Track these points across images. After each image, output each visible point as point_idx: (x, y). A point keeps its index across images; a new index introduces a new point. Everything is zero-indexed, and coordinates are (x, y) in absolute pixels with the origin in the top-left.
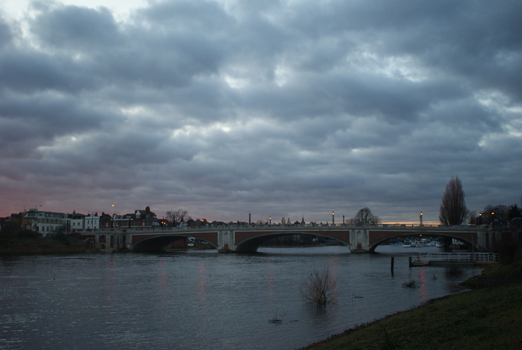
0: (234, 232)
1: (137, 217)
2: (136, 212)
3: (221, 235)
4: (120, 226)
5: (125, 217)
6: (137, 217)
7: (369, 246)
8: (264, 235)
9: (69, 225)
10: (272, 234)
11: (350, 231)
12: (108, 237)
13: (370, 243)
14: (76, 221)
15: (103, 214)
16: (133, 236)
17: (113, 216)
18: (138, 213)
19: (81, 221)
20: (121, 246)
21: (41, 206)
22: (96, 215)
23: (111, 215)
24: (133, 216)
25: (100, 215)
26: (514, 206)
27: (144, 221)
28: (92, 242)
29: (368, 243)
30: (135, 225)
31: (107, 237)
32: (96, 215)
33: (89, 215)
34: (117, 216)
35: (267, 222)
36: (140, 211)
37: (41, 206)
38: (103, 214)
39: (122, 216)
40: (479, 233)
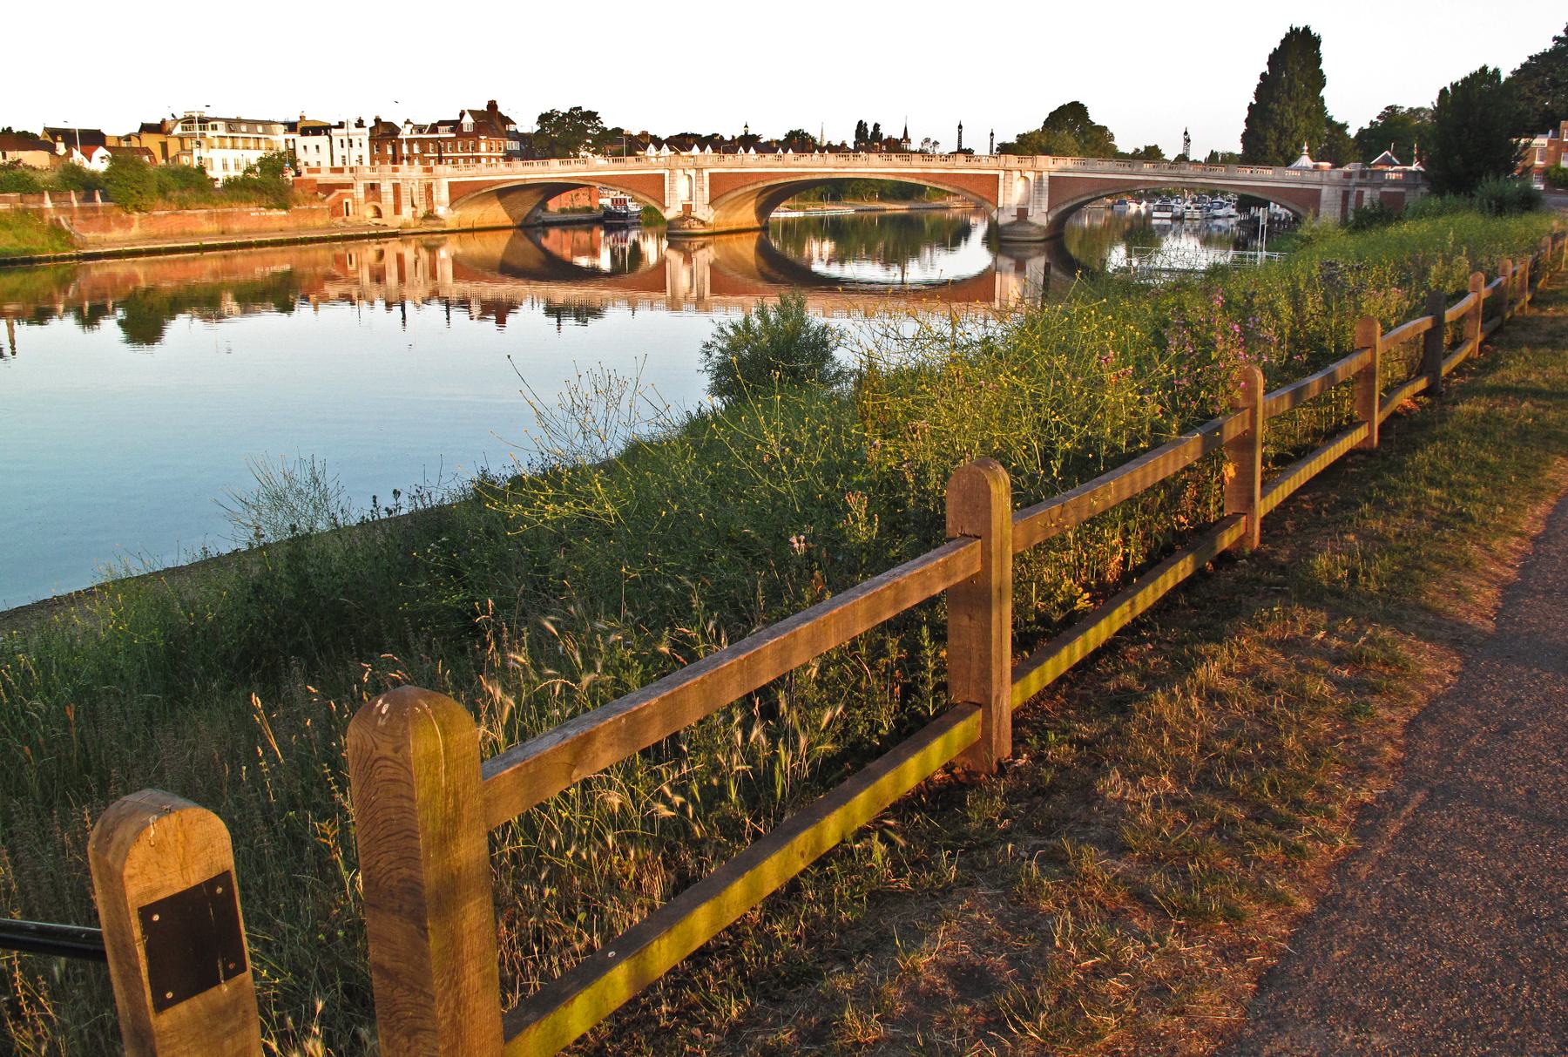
0: (706, 173)
2: (462, 115)
3: (672, 181)
5: (434, 128)
7: (1047, 213)
8: (782, 181)
9: (291, 157)
10: (802, 178)
11: (1002, 174)
12: (386, 188)
13: (1050, 208)
14: (311, 141)
15: (377, 120)
16: (450, 183)
19: (322, 140)
20: (422, 211)
21: (317, 147)
22: (360, 124)
23: (400, 124)
24: (455, 125)
25: (370, 123)
26: (1491, 69)
28: (346, 200)
29: (1045, 208)
31: (383, 189)
32: (360, 124)
33: (341, 125)
35: (978, 568)
36: (471, 112)
37: (317, 147)
38: (377, 120)
39: (426, 127)
40: (1325, 190)
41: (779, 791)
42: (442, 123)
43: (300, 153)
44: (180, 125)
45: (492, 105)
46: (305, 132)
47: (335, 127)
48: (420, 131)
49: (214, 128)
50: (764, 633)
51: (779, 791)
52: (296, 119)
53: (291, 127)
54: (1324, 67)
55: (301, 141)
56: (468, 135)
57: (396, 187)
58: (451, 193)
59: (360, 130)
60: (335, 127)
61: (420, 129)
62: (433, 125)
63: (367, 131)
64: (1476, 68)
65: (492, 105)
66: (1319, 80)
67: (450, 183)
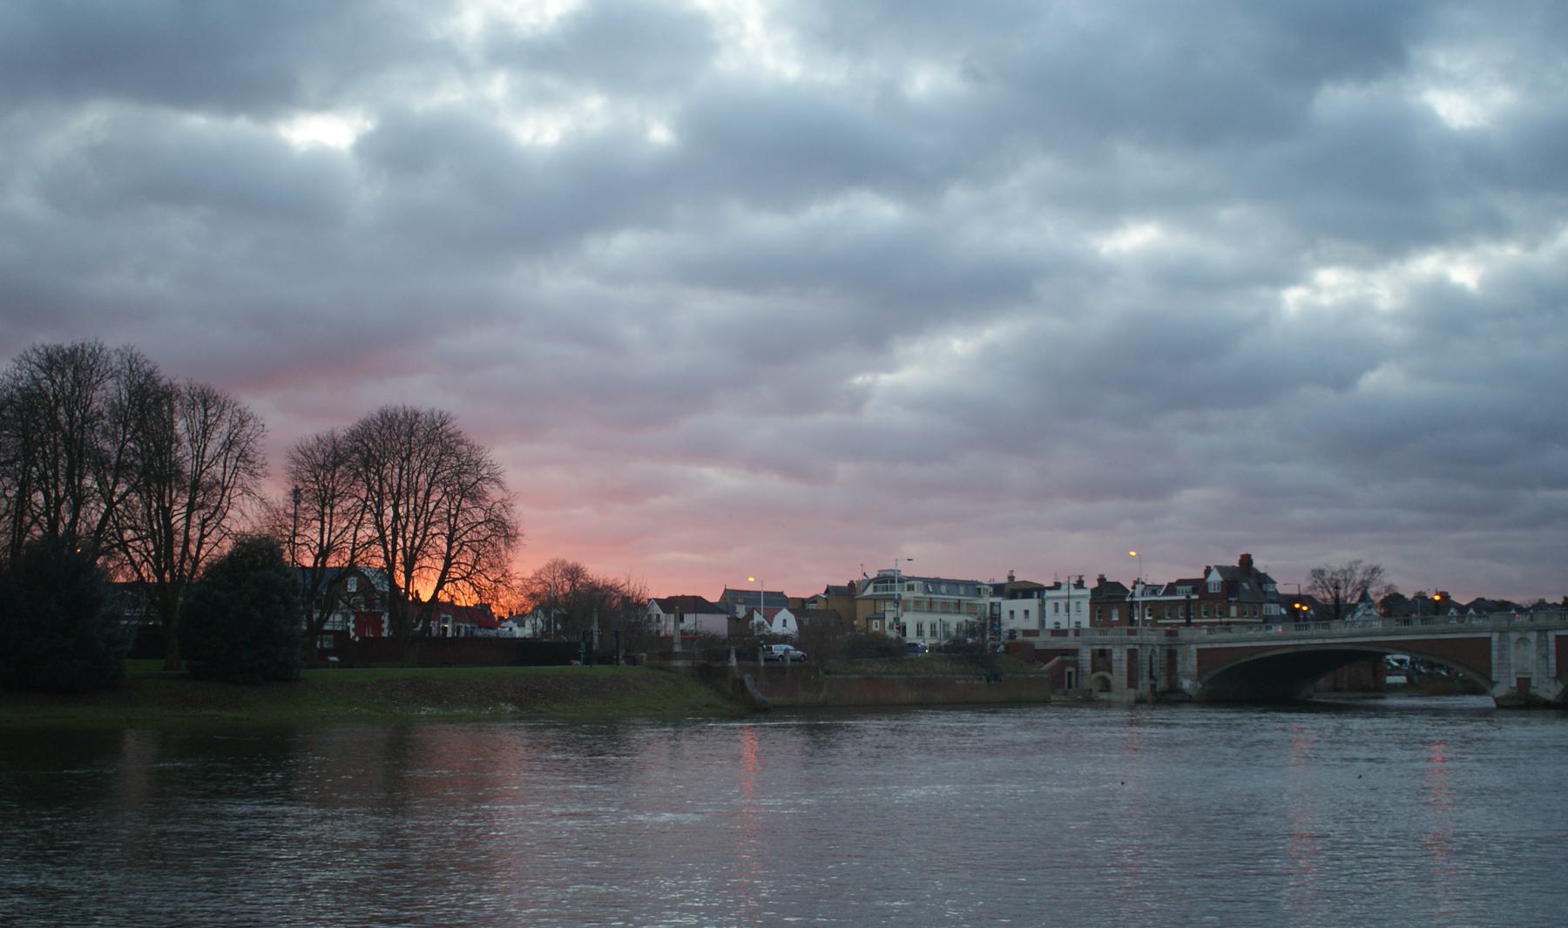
0: (1551, 636)
1: (1211, 590)
2: (1208, 571)
3: (1503, 648)
4: (1159, 618)
5: (1171, 589)
6: (1211, 590)
9: (995, 618)
12: (1119, 656)
14: (1019, 605)
15: (1102, 580)
16: (1199, 651)
17: (1134, 588)
18: (1215, 577)
19: (1032, 604)
22: (1080, 584)
23: (1128, 585)
25: (1092, 583)
27: (1236, 602)
28: (1070, 669)
30: (1206, 613)
32: (1080, 584)
33: (1057, 586)
34: (1147, 586)
38: (1102, 580)
39: (1161, 586)
41: (226, 738)
42: (1181, 582)
43: (1005, 616)
44: (871, 586)
45: (1246, 560)
46: (1013, 595)
47: (1050, 588)
48: (1154, 592)
49: (911, 588)
50: (347, 842)
51: (226, 738)
52: (1004, 580)
53: (998, 590)
54: (679, 595)
55: (1007, 605)
56: (1214, 596)
57: (1132, 654)
58: (1200, 663)
59: (1080, 592)
60: (1050, 588)
61: (1154, 589)
62: (1170, 585)
63: (1088, 592)
64: (781, 591)
65: (1246, 560)
66: (677, 597)
67: (1199, 651)
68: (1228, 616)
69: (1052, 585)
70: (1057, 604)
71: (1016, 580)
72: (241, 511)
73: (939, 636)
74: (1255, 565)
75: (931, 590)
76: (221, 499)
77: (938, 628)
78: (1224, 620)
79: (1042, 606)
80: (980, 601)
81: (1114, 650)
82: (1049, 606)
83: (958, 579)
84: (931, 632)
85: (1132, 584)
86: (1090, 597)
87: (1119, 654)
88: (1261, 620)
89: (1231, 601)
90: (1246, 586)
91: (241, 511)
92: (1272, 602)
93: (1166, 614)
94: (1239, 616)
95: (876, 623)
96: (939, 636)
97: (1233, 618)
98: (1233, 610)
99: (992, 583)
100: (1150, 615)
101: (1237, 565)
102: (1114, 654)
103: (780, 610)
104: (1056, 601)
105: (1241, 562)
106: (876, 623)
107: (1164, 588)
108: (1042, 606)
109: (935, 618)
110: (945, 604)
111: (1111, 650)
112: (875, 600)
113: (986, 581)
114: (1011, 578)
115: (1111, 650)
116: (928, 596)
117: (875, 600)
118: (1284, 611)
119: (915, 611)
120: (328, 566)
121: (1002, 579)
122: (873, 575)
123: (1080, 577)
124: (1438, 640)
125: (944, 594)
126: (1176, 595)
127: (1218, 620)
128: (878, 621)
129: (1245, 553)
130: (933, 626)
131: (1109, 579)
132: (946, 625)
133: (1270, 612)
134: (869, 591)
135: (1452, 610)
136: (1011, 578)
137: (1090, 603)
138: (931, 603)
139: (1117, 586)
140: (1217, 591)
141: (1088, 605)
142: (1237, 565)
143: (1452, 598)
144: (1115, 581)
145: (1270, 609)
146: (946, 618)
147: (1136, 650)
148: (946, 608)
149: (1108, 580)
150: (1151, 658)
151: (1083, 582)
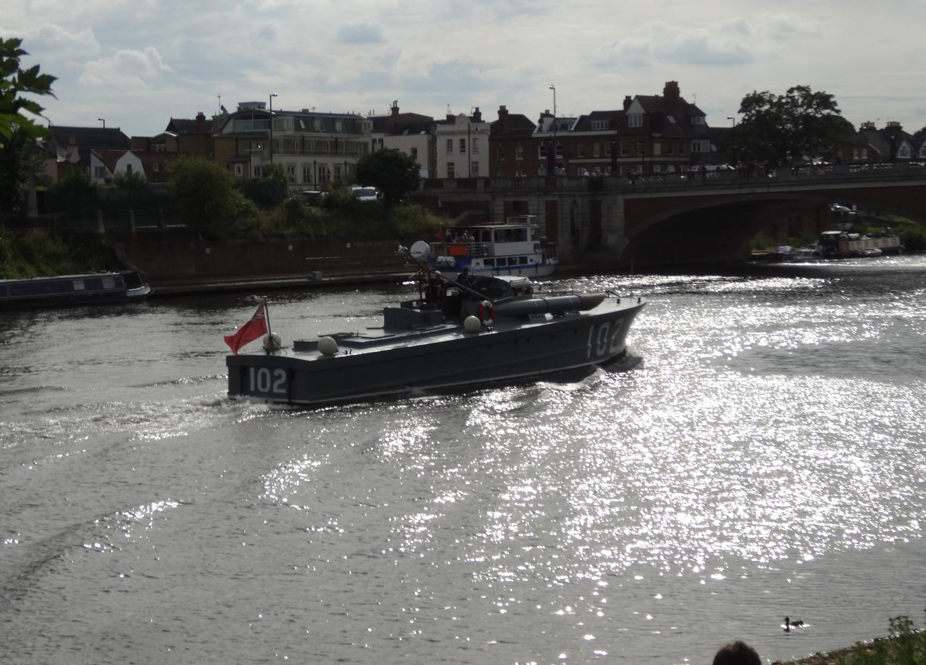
15: (503, 111)
17: (541, 121)
23: (535, 120)
27: (660, 137)
38: (503, 111)
45: (672, 89)
60: (442, 122)
62: (583, 118)
65: (672, 89)
68: (651, 154)
69: (445, 118)
70: (450, 142)
71: (401, 112)
72: (508, 402)
73: (313, 182)
74: (681, 95)
75: (303, 127)
76: (780, 508)
77: (312, 172)
78: (647, 159)
79: (432, 144)
80: (361, 139)
81: (530, 203)
82: (441, 143)
83: (334, 112)
84: (305, 177)
85: (539, 117)
86: (489, 133)
87: (536, 207)
88: (687, 159)
89: (654, 138)
90: (671, 119)
91: (508, 402)
92: (702, 137)
93: (579, 154)
94: (663, 154)
95: (239, 168)
96: (313, 182)
97: (657, 156)
98: (657, 148)
99: (372, 115)
100: (543, 155)
101: (661, 94)
102: (530, 207)
103: (122, 154)
104: (450, 137)
105: (666, 91)
106: (239, 168)
107: (576, 122)
108: (432, 144)
109: (309, 160)
110: (319, 143)
111: (527, 202)
112: (237, 140)
113: (364, 114)
114: (395, 109)
115: (527, 202)
116: (299, 134)
117: (237, 140)
118: (714, 148)
119: (285, 152)
120: (484, 171)
121: (384, 111)
122: (232, 109)
123: (477, 109)
124: (895, 187)
125: (318, 132)
126: (590, 130)
127: (640, 159)
128: (241, 165)
129: (670, 80)
130: (306, 171)
131: (512, 111)
132: (322, 169)
133: (699, 149)
134: (228, 129)
135: (904, 144)
136: (395, 109)
137: (489, 140)
138: (303, 142)
139: (521, 120)
140: (638, 125)
141: (487, 142)
142: (661, 94)
143: (903, 130)
144: (328, 112)
145: (699, 144)
146: (321, 160)
147: (554, 203)
148: (321, 149)
149: (510, 113)
150: (572, 212)
151: (480, 114)
